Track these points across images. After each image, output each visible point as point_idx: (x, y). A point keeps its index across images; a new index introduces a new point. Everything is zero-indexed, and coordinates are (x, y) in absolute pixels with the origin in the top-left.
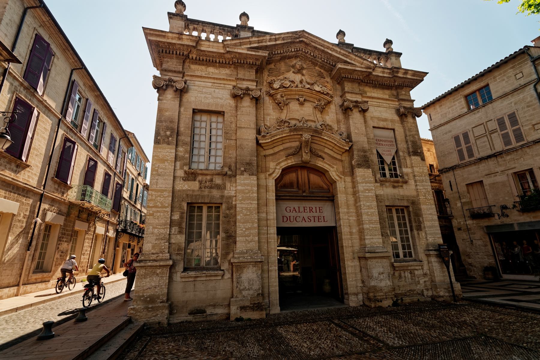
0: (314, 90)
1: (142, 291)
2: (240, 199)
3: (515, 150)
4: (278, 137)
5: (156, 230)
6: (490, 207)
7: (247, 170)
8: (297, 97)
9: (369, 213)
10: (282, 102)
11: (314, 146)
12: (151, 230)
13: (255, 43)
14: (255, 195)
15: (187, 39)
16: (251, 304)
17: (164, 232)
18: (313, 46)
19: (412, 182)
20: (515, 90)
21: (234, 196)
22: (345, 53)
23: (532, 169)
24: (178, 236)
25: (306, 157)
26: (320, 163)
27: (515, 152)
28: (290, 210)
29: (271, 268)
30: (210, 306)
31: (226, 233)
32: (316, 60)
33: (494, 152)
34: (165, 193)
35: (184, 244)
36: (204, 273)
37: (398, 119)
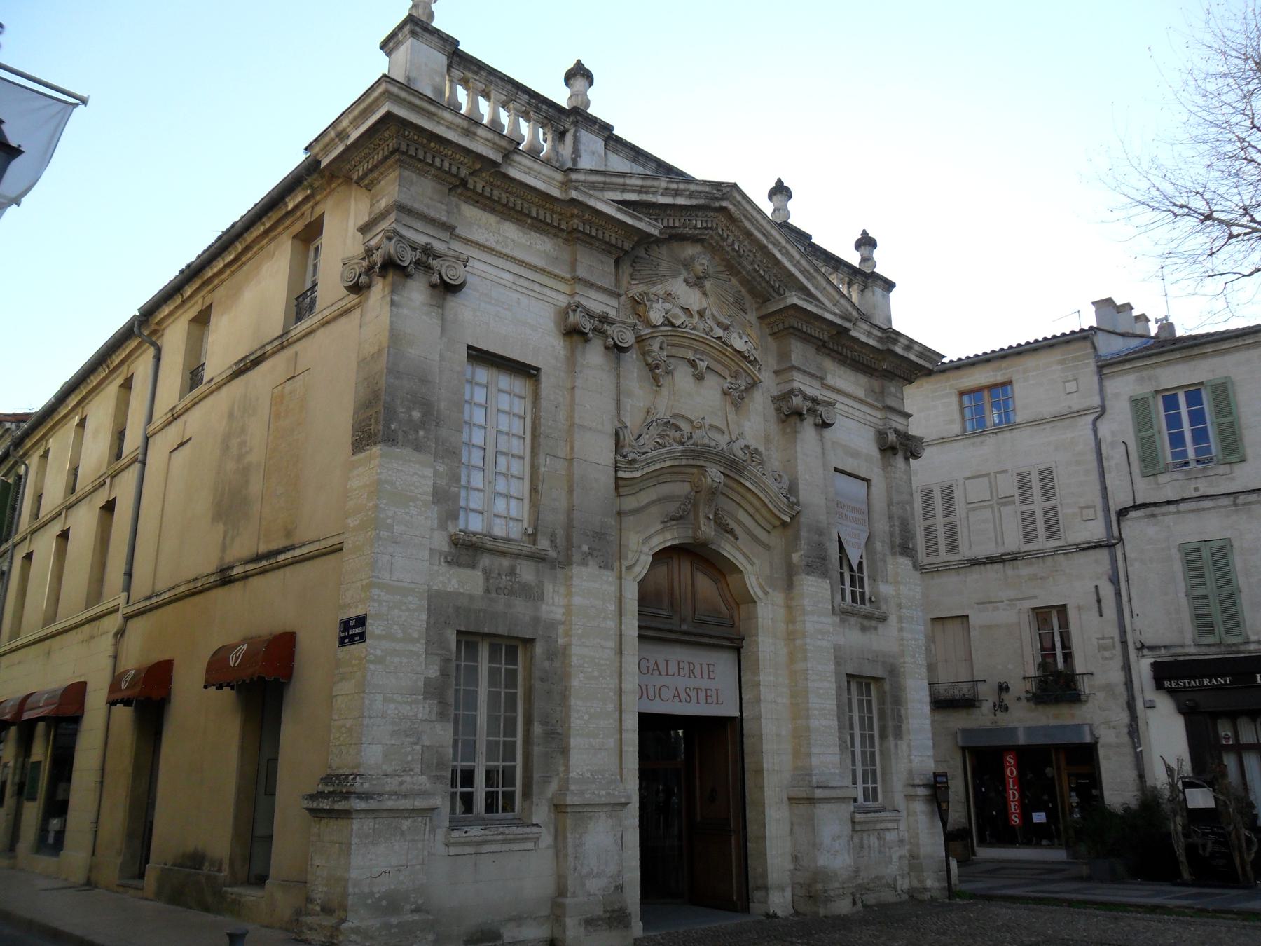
0: (731, 346)
1: (368, 881)
2: (580, 631)
3: (1040, 556)
4: (658, 466)
5: (392, 706)
6: (975, 683)
7: (595, 553)
8: (691, 356)
9: (821, 691)
10: (662, 364)
11: (723, 503)
12: (381, 707)
13: (633, 191)
14: (611, 624)
15: (487, 140)
16: (605, 911)
17: (411, 714)
18: (746, 228)
19: (893, 619)
20: (1060, 417)
21: (563, 623)
22: (808, 267)
23: (1064, 606)
24: (438, 726)
25: (707, 530)
26: (728, 547)
27: (1040, 559)
28: (648, 667)
29: (626, 823)
30: (510, 920)
31: (542, 725)
32: (740, 264)
33: (1001, 550)
34: (410, 598)
35: (451, 751)
36: (502, 834)
37: (879, 456)
